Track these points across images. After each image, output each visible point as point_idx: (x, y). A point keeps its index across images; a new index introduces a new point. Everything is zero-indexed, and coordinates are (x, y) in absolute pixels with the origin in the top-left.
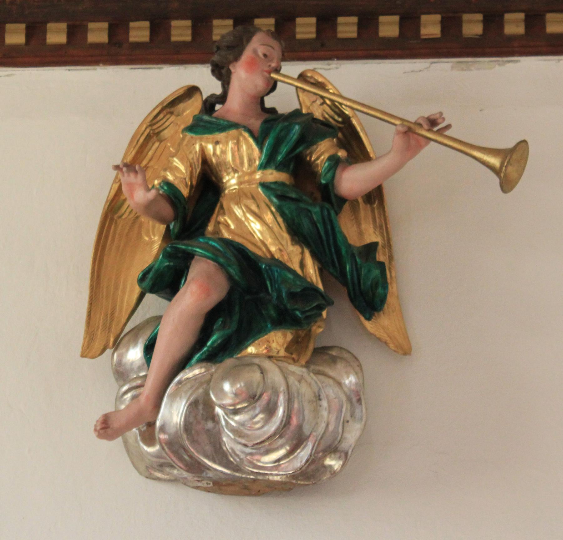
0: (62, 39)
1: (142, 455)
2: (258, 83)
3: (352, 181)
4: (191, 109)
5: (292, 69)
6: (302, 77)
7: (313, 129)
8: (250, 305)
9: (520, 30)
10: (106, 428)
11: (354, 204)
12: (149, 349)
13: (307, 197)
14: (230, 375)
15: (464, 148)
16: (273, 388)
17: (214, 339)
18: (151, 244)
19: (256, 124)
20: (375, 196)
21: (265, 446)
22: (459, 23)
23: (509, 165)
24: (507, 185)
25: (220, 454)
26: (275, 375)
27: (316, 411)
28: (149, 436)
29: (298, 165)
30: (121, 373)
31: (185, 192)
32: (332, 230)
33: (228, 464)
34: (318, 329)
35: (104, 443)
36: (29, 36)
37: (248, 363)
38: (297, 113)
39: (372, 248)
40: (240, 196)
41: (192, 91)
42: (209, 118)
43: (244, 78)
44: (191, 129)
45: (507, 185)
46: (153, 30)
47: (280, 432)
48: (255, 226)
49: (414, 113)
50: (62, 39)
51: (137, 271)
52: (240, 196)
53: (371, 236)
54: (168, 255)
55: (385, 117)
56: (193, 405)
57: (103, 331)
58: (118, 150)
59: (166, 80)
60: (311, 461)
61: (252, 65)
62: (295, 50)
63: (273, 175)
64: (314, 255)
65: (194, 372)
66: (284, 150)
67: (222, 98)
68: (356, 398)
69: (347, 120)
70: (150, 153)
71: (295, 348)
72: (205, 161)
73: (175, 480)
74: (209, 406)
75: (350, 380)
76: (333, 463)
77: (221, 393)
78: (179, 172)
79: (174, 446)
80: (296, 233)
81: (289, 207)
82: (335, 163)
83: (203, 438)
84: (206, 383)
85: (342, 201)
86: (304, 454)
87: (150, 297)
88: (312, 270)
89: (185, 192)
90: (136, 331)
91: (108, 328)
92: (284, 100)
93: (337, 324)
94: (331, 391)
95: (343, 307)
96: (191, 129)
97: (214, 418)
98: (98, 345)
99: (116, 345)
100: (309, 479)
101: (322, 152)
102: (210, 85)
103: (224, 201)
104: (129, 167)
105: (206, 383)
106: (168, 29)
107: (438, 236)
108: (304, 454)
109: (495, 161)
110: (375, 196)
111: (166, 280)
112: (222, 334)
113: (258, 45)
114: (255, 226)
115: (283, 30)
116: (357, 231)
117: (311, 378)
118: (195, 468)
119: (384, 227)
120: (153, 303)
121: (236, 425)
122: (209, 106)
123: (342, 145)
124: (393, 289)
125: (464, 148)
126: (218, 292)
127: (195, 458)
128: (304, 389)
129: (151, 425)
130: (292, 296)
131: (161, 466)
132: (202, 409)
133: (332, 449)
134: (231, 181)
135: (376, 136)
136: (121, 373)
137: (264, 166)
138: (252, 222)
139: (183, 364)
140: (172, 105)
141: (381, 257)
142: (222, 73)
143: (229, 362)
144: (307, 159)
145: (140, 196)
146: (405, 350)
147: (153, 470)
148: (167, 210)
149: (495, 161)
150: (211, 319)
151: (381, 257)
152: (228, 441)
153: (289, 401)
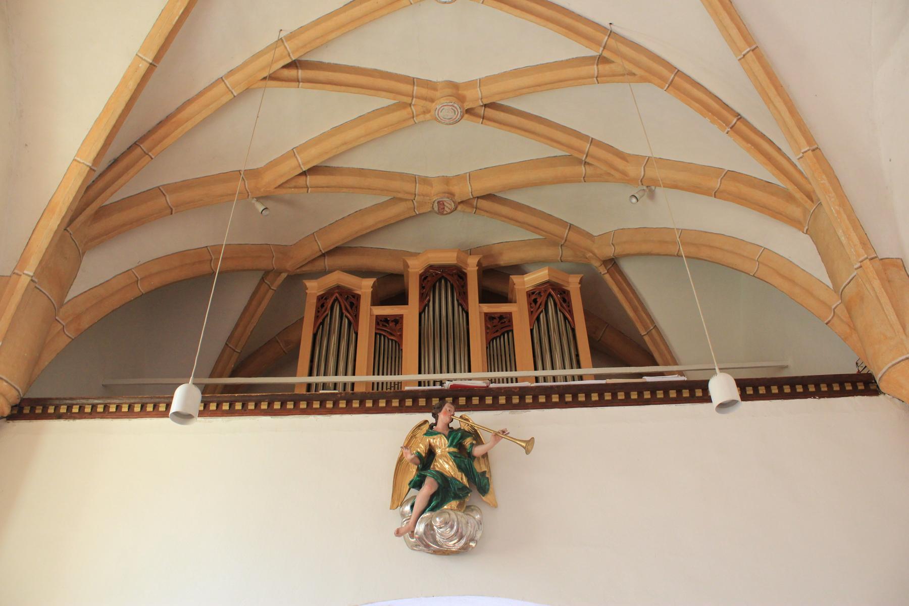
0: (384, 405)
1: (410, 542)
2: (448, 419)
3: (478, 451)
4: (426, 428)
5: (458, 414)
6: (461, 417)
7: (465, 434)
8: (445, 493)
9: (531, 401)
10: (398, 533)
11: (479, 458)
12: (412, 507)
13: (463, 457)
14: (439, 515)
15: (513, 440)
16: (466, 252)
17: (433, 504)
18: (412, 472)
19: (447, 433)
20: (485, 456)
21: (450, 539)
22: (511, 399)
23: (529, 445)
24: (528, 452)
25: (435, 542)
26: (453, 516)
27: (467, 527)
28: (412, 536)
29: (460, 446)
30: (403, 515)
31: (424, 455)
32: (471, 467)
33: (438, 545)
34: (467, 500)
35: (398, 538)
36: (373, 404)
37: (444, 512)
38: (460, 429)
39: (484, 473)
40: (441, 456)
41: (426, 422)
42: (432, 431)
43: (443, 418)
44: (425, 434)
45: (528, 452)
46: (413, 402)
47: (455, 534)
48: (447, 466)
49: (498, 429)
50: (384, 405)
51: (408, 482)
52: (441, 456)
53: (484, 469)
54: (418, 476)
55: (488, 430)
56: (427, 526)
57: (397, 501)
58: (402, 441)
59: (417, 418)
60: (466, 544)
61: (445, 413)
62: (459, 408)
63: (452, 449)
64: (466, 476)
65: (427, 514)
66: (456, 441)
67: (436, 424)
68: (480, 523)
69: (476, 431)
70: (631, 314)
71: (460, 506)
72: (430, 445)
73: (420, 550)
74: (432, 526)
75: (478, 517)
76: (473, 544)
77: (436, 521)
78: (422, 449)
79: (420, 539)
80: (460, 468)
81: (458, 460)
82: (472, 445)
83: (430, 537)
84: (431, 518)
85: (474, 457)
86: (463, 541)
87: (412, 490)
88: (465, 480)
89: (424, 455)
90: (408, 501)
91: (398, 500)
92: (455, 425)
93: (473, 498)
94: (471, 521)
95: (475, 492)
96: (425, 434)
97: (433, 530)
98: (395, 506)
99: (401, 505)
100: (465, 549)
101: (468, 442)
102: (432, 420)
103: (436, 458)
104: (406, 447)
105: (431, 518)
106: (418, 402)
107: (503, 466)
108: (463, 541)
109: (524, 444)
110: (485, 456)
111: (417, 484)
112: (435, 502)
113: (447, 407)
114: (447, 466)
115: (455, 402)
116: (479, 467)
117: (465, 516)
118: (427, 546)
119: (488, 466)
120: (413, 491)
121: (442, 533)
122: (431, 427)
123: (474, 439)
124: (491, 486)
125: (513, 440)
126: (435, 488)
127: (427, 543)
128: (464, 521)
129: (413, 532)
130: (459, 489)
131: (416, 546)
132: (429, 527)
133: (472, 540)
134: (438, 451)
135: (485, 436)
136: (403, 515)
137: (449, 446)
138: (445, 465)
139: (423, 512)
140: (419, 426)
141: (487, 476)
142: (435, 416)
143: (438, 511)
144: (463, 444)
145: (409, 457)
146: (495, 506)
147: (413, 547)
148: (418, 461)
149: (524, 444)
150: (432, 497)
151: (487, 476)
152: (438, 537)
153: (458, 524)
